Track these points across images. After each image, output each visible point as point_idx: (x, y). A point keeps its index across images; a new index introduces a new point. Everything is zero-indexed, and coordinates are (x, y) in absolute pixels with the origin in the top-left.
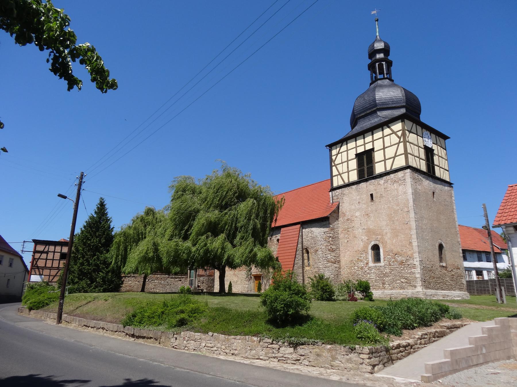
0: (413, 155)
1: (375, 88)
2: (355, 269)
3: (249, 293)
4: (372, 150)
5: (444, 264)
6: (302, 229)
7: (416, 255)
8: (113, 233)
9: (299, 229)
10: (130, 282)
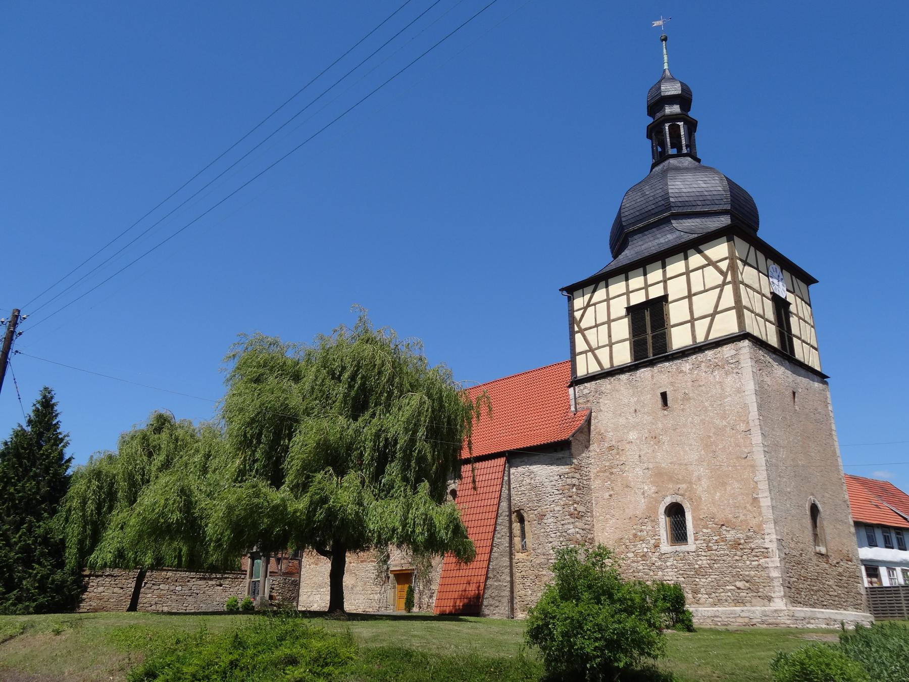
0: (752, 312)
1: (665, 172)
3: (383, 612)
4: (664, 299)
5: (823, 550)
6: (510, 467)
7: (769, 528)
8: (69, 472)
9: (501, 468)
10: (101, 589)
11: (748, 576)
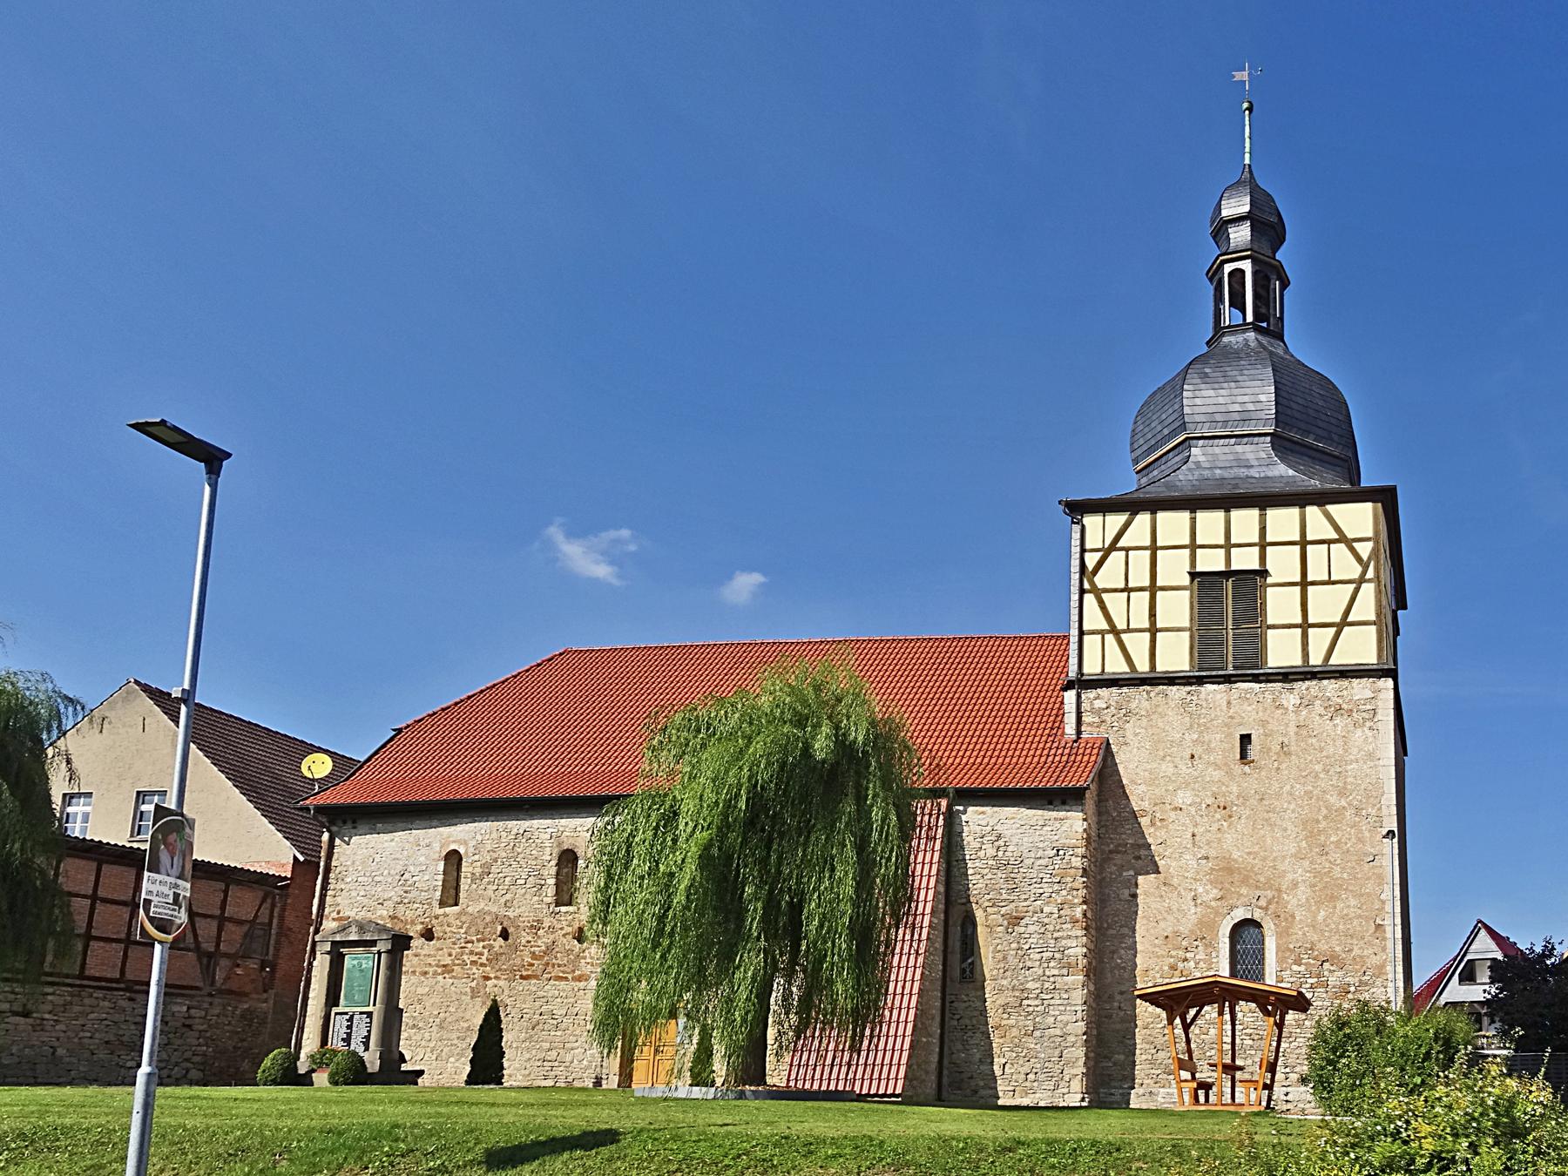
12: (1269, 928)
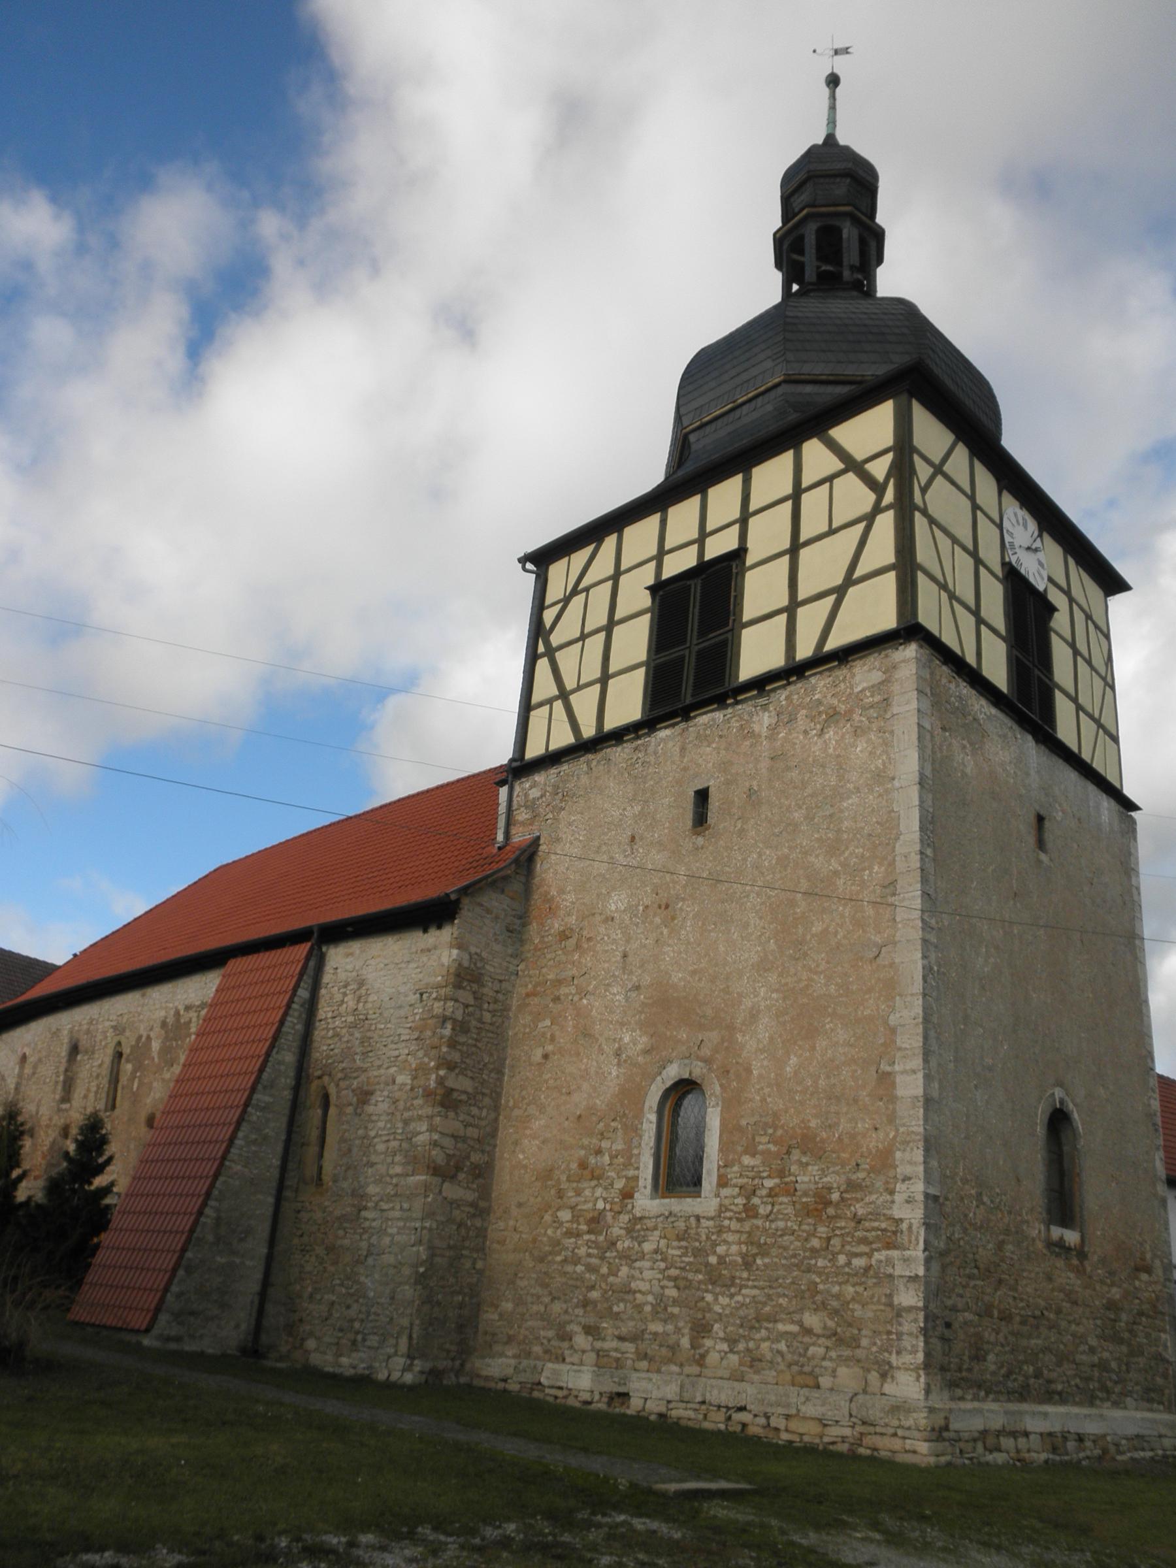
0: (943, 587)
2: (558, 1223)
4: (739, 554)
5: (1071, 1237)
7: (911, 1161)
11: (837, 1297)
12: (713, 1088)
